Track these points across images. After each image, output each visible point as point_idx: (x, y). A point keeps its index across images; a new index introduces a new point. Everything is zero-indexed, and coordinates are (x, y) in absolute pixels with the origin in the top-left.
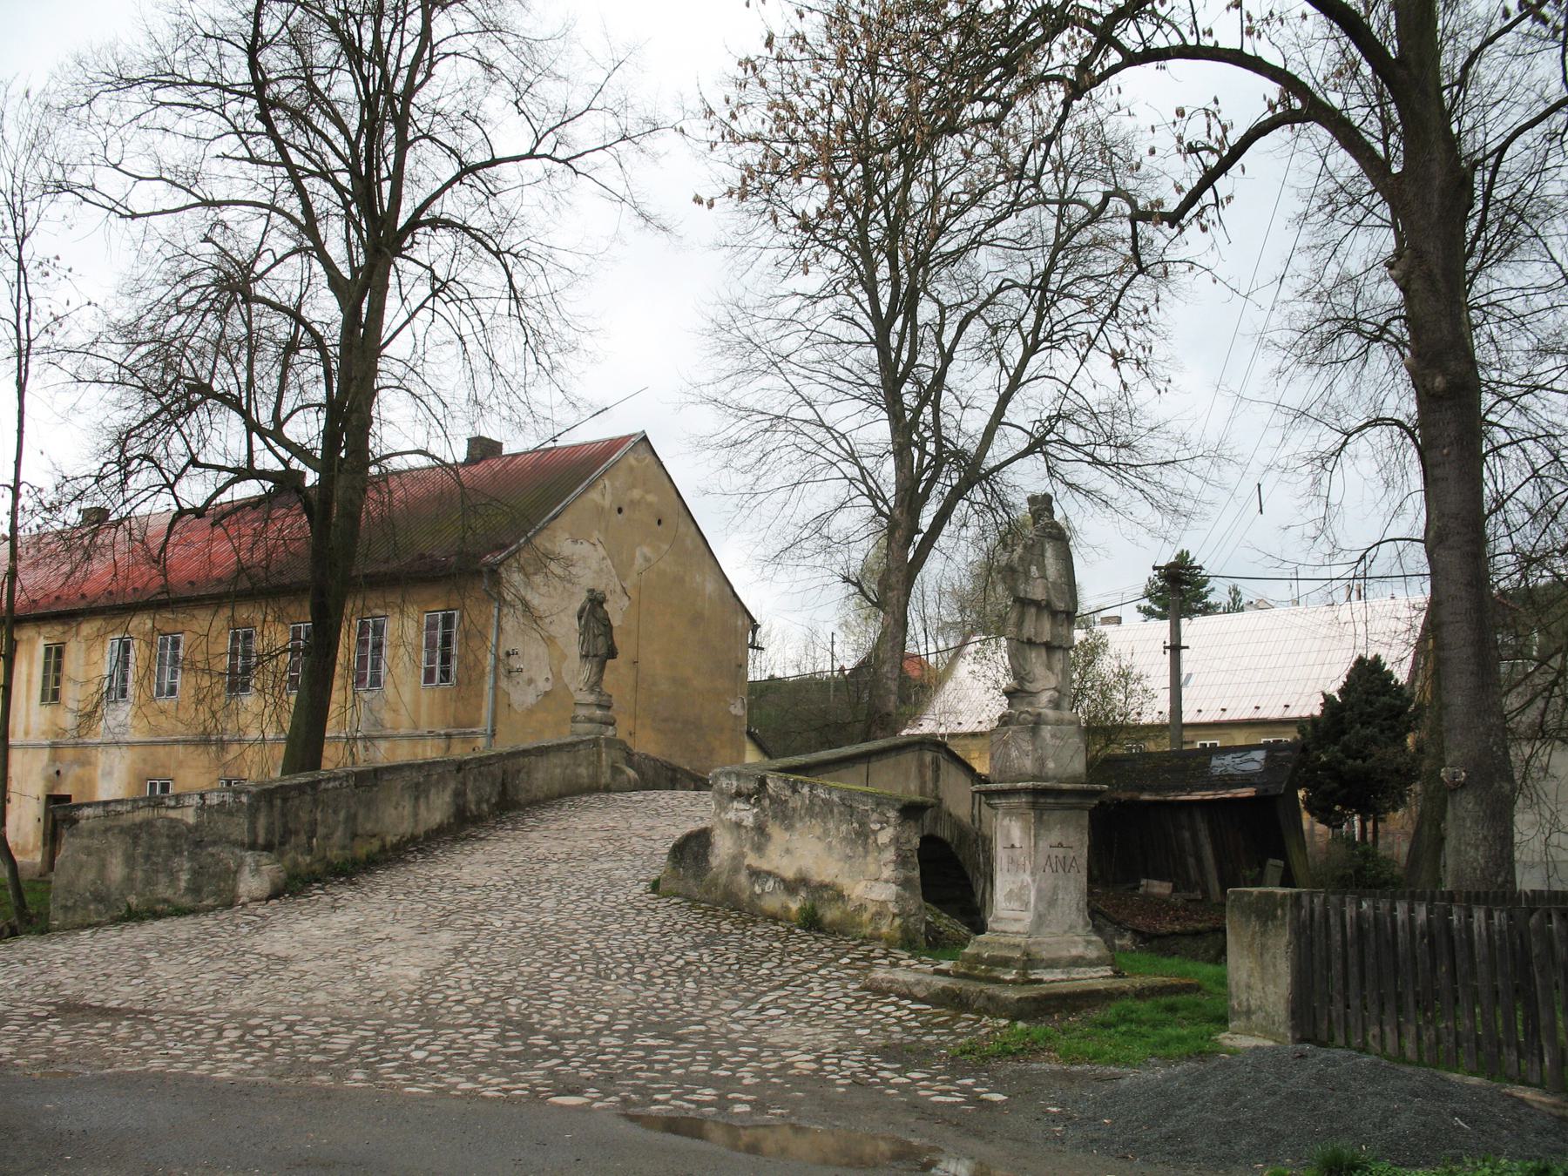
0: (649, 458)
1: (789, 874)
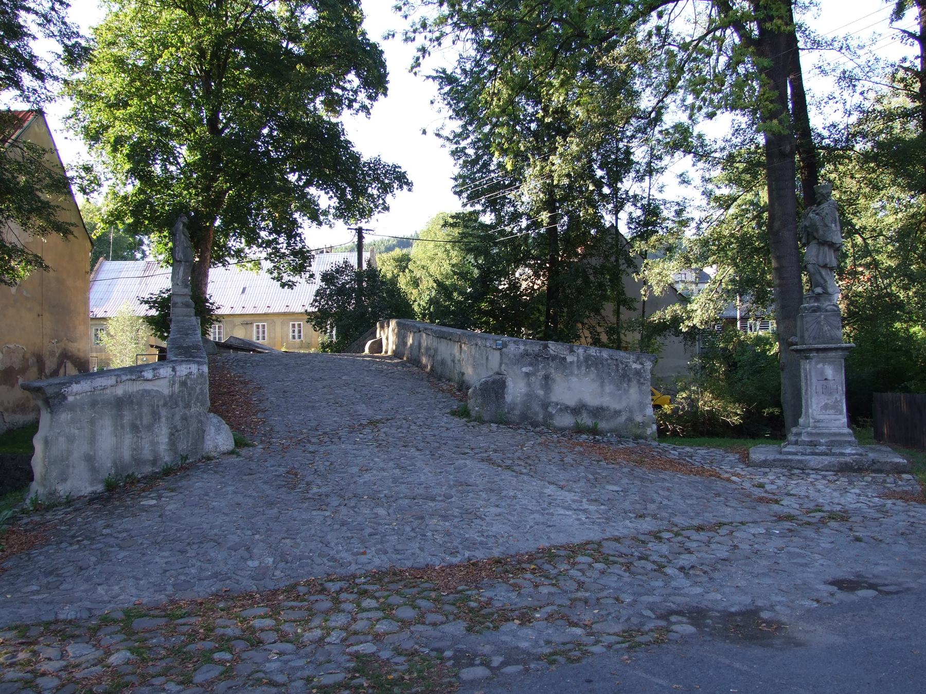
0: (45, 127)
1: (571, 402)
